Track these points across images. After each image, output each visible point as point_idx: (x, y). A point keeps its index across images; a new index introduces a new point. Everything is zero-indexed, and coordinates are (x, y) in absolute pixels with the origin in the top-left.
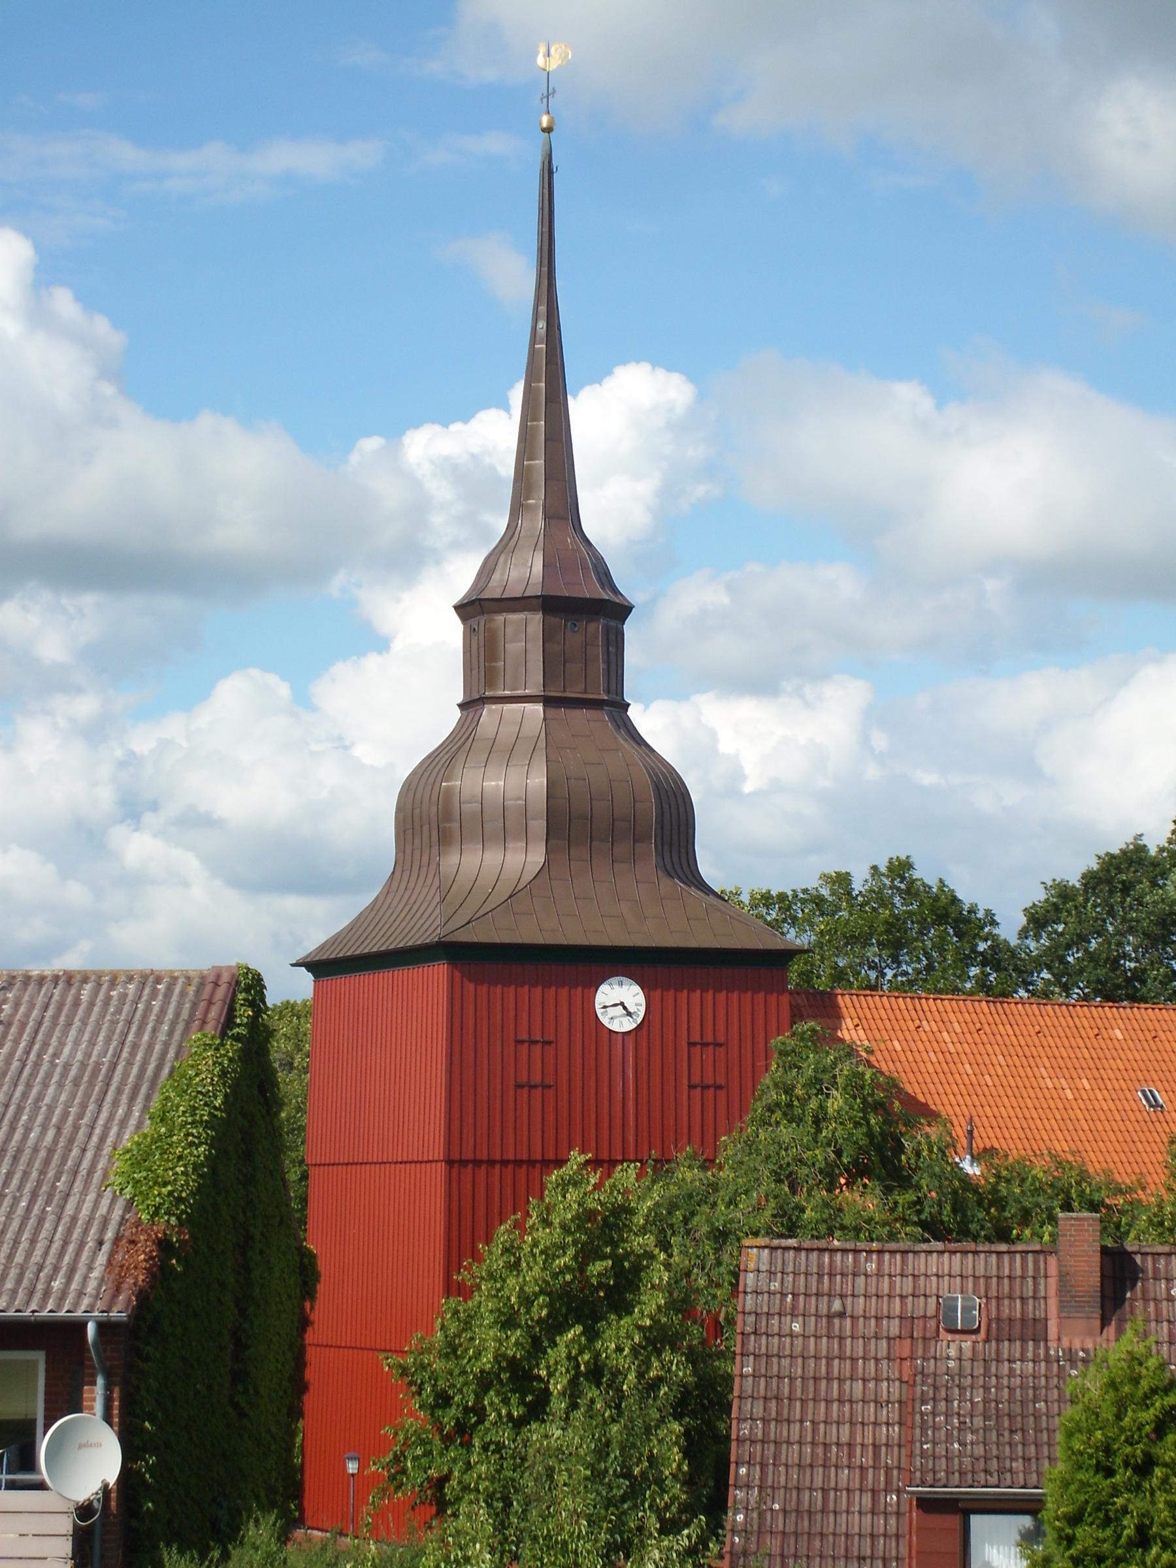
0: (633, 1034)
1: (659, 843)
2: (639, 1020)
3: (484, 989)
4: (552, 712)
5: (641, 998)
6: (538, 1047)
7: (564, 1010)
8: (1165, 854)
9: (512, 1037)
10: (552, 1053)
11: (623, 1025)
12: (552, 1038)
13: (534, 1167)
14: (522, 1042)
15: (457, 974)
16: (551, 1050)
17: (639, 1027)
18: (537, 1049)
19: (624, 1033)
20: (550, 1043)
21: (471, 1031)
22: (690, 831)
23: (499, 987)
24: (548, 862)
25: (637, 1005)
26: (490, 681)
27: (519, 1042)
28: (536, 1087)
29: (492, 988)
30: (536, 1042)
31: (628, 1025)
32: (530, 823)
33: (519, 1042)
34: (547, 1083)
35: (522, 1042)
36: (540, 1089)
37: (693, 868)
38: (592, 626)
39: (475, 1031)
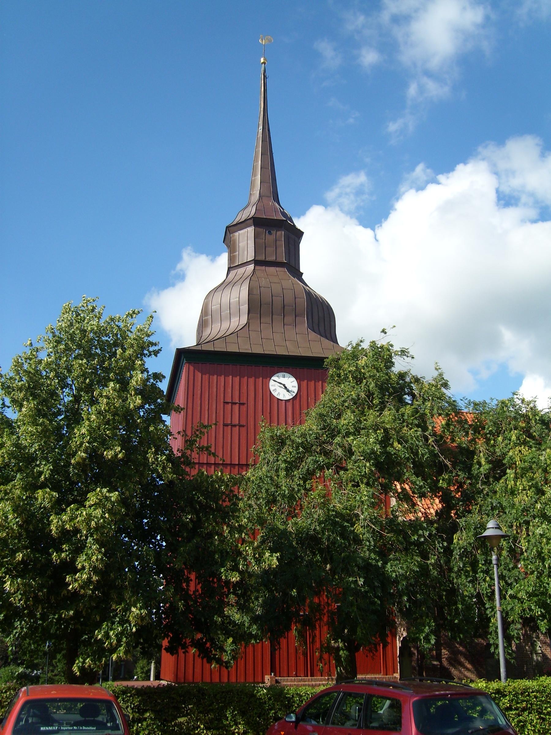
0: (291, 401)
1: (310, 317)
2: (294, 394)
3: (206, 377)
4: (258, 268)
5: (295, 383)
6: (236, 407)
7: (251, 388)
8: (258, 641)
9: (222, 401)
10: (245, 409)
11: (284, 395)
12: (245, 401)
13: (234, 468)
14: (228, 403)
15: (192, 368)
16: (244, 408)
17: (294, 398)
18: (236, 407)
19: (285, 400)
20: (244, 404)
21: (199, 396)
22: (332, 323)
23: (215, 376)
24: (248, 323)
25: (293, 387)
26: (234, 263)
27: (226, 403)
28: (235, 426)
29: (211, 376)
30: (236, 403)
31: (288, 396)
32: (241, 307)
33: (226, 403)
34: (241, 423)
35: (228, 403)
36: (238, 427)
37: (333, 336)
38: (279, 233)
39: (201, 396)
